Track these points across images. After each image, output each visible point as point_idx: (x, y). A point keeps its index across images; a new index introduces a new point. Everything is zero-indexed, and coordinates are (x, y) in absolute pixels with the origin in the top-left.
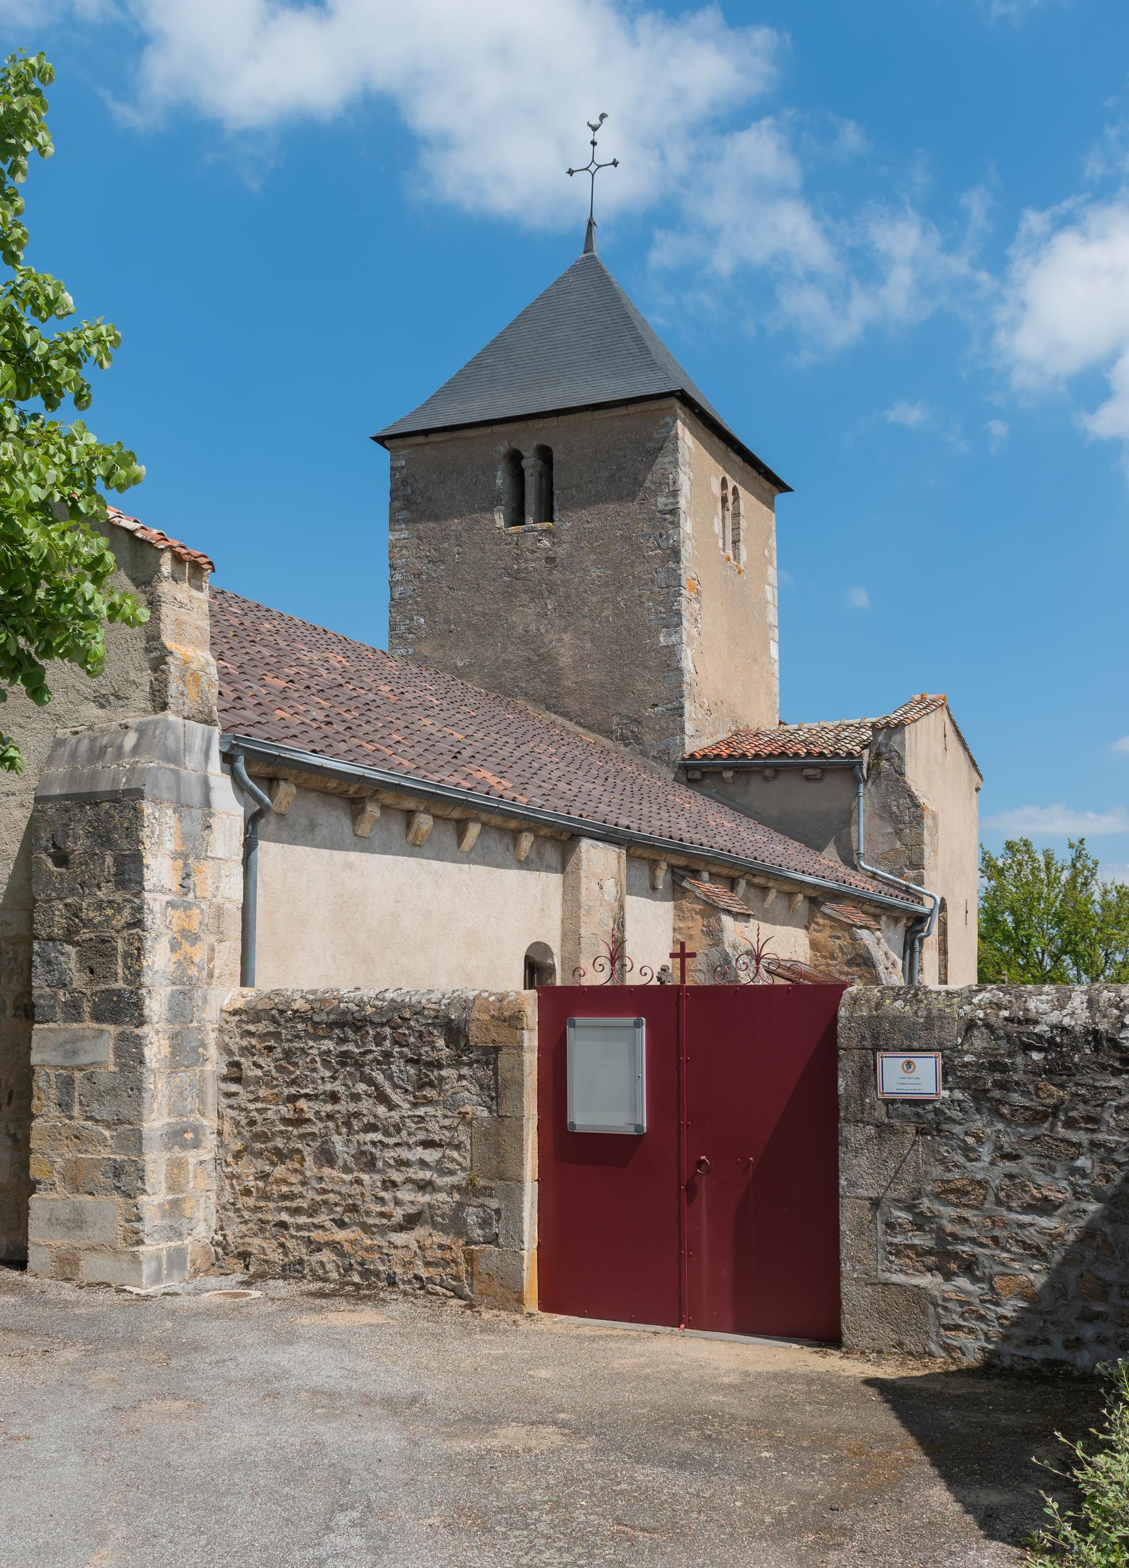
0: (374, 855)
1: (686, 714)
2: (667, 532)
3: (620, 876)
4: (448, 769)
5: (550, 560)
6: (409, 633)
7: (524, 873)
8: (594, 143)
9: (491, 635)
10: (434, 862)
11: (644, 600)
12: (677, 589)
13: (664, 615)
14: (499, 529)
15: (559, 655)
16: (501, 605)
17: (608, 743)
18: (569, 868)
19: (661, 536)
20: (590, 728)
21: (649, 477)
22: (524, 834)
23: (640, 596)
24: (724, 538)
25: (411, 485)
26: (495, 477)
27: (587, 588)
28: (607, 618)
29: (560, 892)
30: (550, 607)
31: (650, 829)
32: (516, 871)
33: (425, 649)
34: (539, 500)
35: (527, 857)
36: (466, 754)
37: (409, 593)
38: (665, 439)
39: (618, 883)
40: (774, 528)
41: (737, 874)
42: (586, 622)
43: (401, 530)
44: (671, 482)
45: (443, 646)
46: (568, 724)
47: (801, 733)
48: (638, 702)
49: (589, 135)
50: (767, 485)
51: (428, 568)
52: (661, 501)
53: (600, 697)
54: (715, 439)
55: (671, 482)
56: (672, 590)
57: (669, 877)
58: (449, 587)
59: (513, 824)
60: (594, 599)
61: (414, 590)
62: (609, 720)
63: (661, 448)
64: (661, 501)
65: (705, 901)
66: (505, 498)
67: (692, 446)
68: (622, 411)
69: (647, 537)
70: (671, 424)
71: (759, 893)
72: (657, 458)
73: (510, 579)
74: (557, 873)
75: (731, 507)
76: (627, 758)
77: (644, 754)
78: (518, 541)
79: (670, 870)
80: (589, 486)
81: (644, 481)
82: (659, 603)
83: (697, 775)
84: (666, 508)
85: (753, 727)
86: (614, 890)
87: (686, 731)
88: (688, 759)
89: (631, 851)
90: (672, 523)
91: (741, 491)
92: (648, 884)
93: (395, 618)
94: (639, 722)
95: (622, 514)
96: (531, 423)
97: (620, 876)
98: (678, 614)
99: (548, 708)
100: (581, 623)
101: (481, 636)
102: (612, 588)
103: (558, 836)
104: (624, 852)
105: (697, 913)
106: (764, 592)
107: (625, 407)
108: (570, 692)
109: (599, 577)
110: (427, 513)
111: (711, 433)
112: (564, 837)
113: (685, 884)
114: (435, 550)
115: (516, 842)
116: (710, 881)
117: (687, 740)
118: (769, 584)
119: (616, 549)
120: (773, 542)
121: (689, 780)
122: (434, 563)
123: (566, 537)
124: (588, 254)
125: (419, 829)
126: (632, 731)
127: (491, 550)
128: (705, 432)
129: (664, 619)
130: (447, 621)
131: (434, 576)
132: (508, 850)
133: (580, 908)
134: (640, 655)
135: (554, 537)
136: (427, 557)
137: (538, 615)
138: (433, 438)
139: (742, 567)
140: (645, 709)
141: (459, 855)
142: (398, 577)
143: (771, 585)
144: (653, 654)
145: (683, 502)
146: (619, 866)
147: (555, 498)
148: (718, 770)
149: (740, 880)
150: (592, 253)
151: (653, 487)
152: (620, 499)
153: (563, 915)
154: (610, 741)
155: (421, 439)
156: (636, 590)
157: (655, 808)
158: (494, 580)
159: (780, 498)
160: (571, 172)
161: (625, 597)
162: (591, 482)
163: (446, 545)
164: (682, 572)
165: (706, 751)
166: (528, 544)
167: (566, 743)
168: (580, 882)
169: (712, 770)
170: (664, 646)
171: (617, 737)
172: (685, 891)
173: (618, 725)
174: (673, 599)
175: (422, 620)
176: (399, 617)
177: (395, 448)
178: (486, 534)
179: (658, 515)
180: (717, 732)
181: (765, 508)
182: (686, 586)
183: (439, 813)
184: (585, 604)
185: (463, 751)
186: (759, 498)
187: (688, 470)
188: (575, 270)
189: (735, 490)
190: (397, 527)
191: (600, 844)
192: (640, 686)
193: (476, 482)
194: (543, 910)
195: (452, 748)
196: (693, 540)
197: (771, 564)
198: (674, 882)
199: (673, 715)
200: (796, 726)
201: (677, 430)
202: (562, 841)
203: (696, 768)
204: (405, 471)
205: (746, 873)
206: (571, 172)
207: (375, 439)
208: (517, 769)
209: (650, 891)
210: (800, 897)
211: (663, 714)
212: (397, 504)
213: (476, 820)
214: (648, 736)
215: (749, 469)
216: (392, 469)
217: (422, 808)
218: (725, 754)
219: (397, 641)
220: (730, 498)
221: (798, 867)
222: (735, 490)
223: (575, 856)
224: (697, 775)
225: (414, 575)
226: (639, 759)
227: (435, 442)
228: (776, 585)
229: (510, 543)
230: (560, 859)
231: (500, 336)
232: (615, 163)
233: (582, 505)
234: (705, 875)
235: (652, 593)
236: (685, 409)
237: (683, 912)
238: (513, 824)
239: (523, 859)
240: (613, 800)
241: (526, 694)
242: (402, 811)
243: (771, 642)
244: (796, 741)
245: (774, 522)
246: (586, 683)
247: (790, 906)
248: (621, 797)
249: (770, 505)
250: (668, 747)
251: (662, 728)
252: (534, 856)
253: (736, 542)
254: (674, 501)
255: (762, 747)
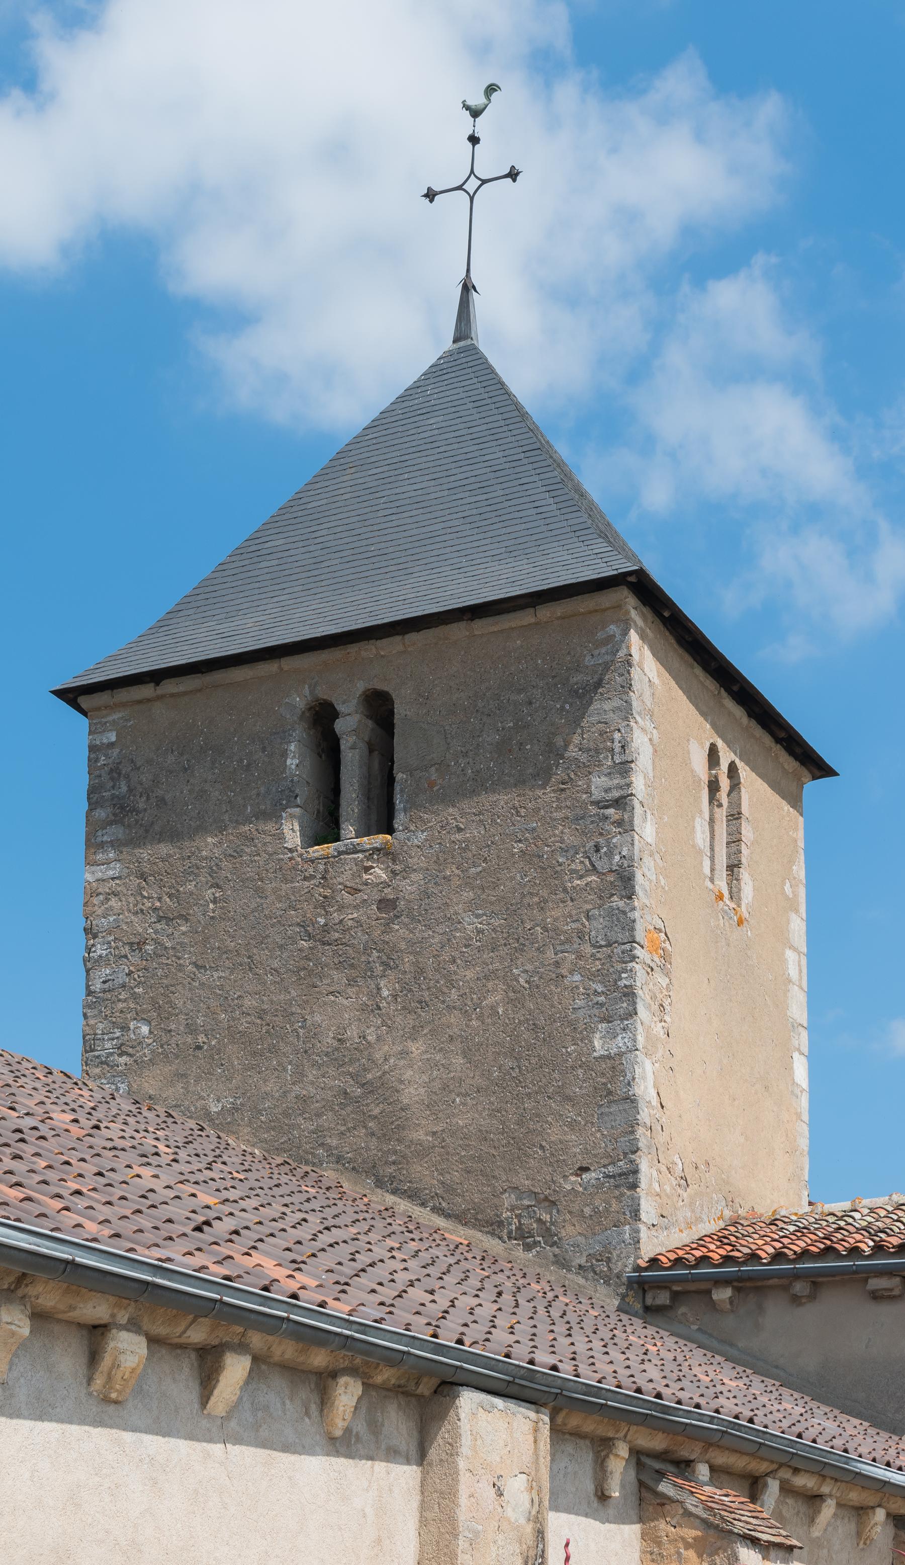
0: (15, 1422)
1: (643, 1183)
2: (608, 842)
3: (537, 1470)
4: (182, 1245)
5: (386, 904)
6: (120, 1055)
7: (341, 1463)
8: (474, 140)
9: (274, 1050)
10: (147, 1438)
11: (564, 972)
12: (628, 947)
13: (602, 999)
14: (291, 850)
15: (401, 1082)
16: (294, 993)
17: (494, 1245)
18: (433, 1453)
19: (597, 849)
20: (460, 1218)
21: (576, 739)
22: (343, 1380)
23: (557, 964)
24: (712, 858)
25: (127, 777)
26: (284, 754)
27: (456, 954)
28: (493, 1009)
29: (415, 1500)
30: (385, 993)
31: (598, 1376)
32: (324, 1458)
33: (150, 1084)
34: (367, 795)
35: (348, 1430)
36: (222, 1228)
37: (121, 978)
38: (607, 667)
39: (533, 1485)
40: (801, 844)
41: (764, 1467)
42: (454, 1018)
43: (108, 863)
44: (617, 746)
45: (184, 1076)
46: (417, 1211)
47: (857, 1215)
48: (551, 1164)
49: (466, 124)
50: (790, 764)
51: (156, 932)
52: (599, 784)
53: (480, 1159)
54: (698, 671)
55: (617, 746)
56: (618, 950)
57: (632, 1474)
58: (195, 964)
59: (319, 1359)
60: (470, 974)
61: (129, 974)
62: (496, 1200)
63: (599, 684)
64: (599, 784)
65: (704, 1521)
66: (303, 793)
67: (656, 681)
68: (526, 618)
69: (572, 852)
70: (618, 638)
71: (802, 1507)
72: (590, 703)
73: (311, 944)
74: (408, 1463)
75: (725, 801)
76: (531, 1271)
77: (562, 1262)
78: (326, 871)
79: (634, 1461)
80: (462, 762)
81: (566, 746)
82: (592, 976)
83: (663, 1298)
84: (609, 796)
85: (765, 1210)
86: (525, 1499)
87: (643, 1216)
88: (646, 1269)
89: (559, 1420)
90: (619, 823)
91: (744, 772)
92: (590, 1487)
93: (93, 1027)
94: (553, 1203)
95: (523, 812)
96: (353, 649)
97: (537, 1470)
98: (629, 994)
99: (379, 1183)
100: (444, 1020)
101: (254, 1054)
102: (503, 951)
103: (411, 1387)
104: (547, 1419)
105: (688, 1546)
106: (784, 961)
107: (532, 610)
108: (423, 1152)
109: (480, 931)
110: (157, 828)
111: (690, 660)
112: (425, 1388)
113: (665, 1487)
114: (170, 896)
115: (324, 1398)
116: (712, 1482)
117: (644, 1234)
118: (792, 947)
119: (512, 878)
120: (799, 870)
121: (647, 1309)
122: (169, 920)
123: (417, 860)
124: (462, 344)
125: (116, 1365)
126: (539, 1221)
127: (275, 891)
128: (679, 657)
129: (602, 1005)
130: (192, 1029)
131: (169, 945)
132: (307, 1413)
133: (456, 1536)
134: (556, 1075)
135: (394, 861)
136: (155, 909)
137: (364, 1008)
138: (169, 686)
139: (745, 915)
140: (565, 1177)
141: (204, 1423)
142: (100, 950)
143: (795, 949)
144: (580, 1072)
145: (639, 784)
146: (536, 1449)
147: (397, 788)
148: (703, 1286)
149: (770, 1481)
150: (469, 342)
151: (583, 758)
152: (520, 782)
153: (421, 1552)
154: (496, 1241)
155: (146, 691)
156: (550, 954)
157: (597, 1344)
158: (281, 947)
159: (813, 788)
160: (431, 195)
161: (529, 967)
162: (465, 755)
163: (191, 887)
164: (636, 914)
165: (680, 1253)
166: (346, 878)
167: (417, 1238)
168: (456, 1481)
169: (692, 1287)
170: (602, 1057)
171: (510, 1232)
172: (664, 1501)
173: (512, 1210)
174: (619, 967)
175: (145, 1029)
176: (101, 1026)
177: (98, 709)
178: (267, 862)
179: (593, 810)
180: (699, 1220)
181: (786, 807)
182: (645, 943)
183: (161, 1330)
184: (451, 984)
185: (215, 1223)
186: (775, 786)
187: (649, 725)
188: (436, 372)
189: (733, 770)
190: (100, 857)
191: (498, 1402)
192: (555, 1133)
193: (249, 765)
194: (379, 1541)
195: (192, 1215)
196: (657, 857)
197: (797, 911)
198: (641, 1484)
199: (616, 1187)
200: (847, 1205)
201: (628, 647)
202: (420, 1397)
203: (661, 1284)
204: (115, 752)
205: (781, 1465)
206: (431, 195)
207: (54, 692)
208: (327, 1260)
209: (595, 1504)
210: (880, 1515)
211: (599, 1186)
212: (101, 814)
213: (242, 1347)
214: (569, 1228)
215: (759, 731)
216: (92, 748)
217: (123, 1318)
218: (716, 1257)
219: (97, 1071)
220: (725, 783)
221: (878, 1454)
222: (733, 770)
223: (446, 1426)
224: (663, 1298)
225: (131, 944)
226: (552, 1273)
227: (172, 695)
228: (804, 950)
229: (312, 877)
230: (415, 1434)
231: (298, 498)
232: (513, 175)
233: (448, 797)
234: (703, 1471)
235: (580, 957)
236: (644, 610)
237: (659, 1544)
238: (319, 1359)
239: (338, 1433)
240: (516, 1326)
241: (339, 1159)
242: (80, 1326)
243: (796, 1055)
244: (849, 1228)
245: (801, 834)
246: (453, 1134)
247: (859, 1534)
248: (532, 1322)
249: (795, 801)
250: (607, 1247)
251: (596, 1211)
252: (361, 1427)
253: (733, 868)
254: (623, 782)
255: (786, 1241)
